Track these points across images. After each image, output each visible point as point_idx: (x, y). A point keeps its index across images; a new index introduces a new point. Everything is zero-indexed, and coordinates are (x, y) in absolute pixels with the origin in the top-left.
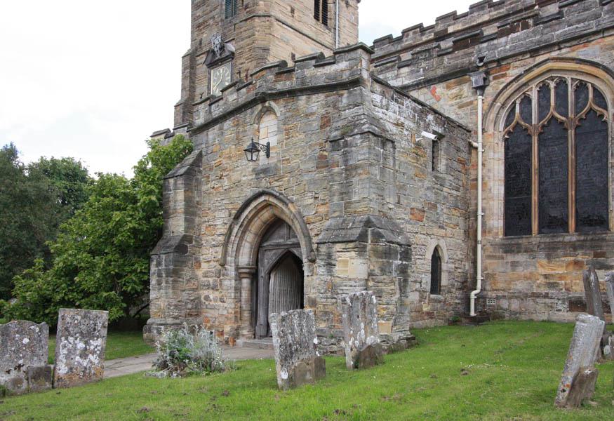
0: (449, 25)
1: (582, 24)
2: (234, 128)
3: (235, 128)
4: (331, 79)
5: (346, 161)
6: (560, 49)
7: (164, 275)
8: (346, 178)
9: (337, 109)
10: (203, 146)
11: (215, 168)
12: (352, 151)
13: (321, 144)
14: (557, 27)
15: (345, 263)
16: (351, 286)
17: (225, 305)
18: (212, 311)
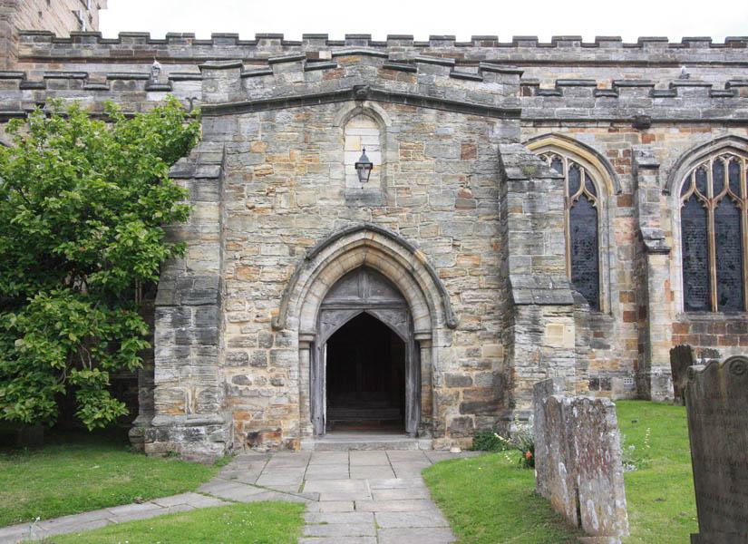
1: (579, 109)
3: (302, 125)
4: (476, 99)
5: (533, 208)
6: (561, 127)
7: (195, 341)
8: (534, 228)
9: (485, 138)
10: (229, 138)
11: (254, 177)
12: (540, 196)
13: (461, 179)
14: (557, 104)
15: (559, 329)
16: (568, 357)
17: (284, 389)
18: (255, 401)
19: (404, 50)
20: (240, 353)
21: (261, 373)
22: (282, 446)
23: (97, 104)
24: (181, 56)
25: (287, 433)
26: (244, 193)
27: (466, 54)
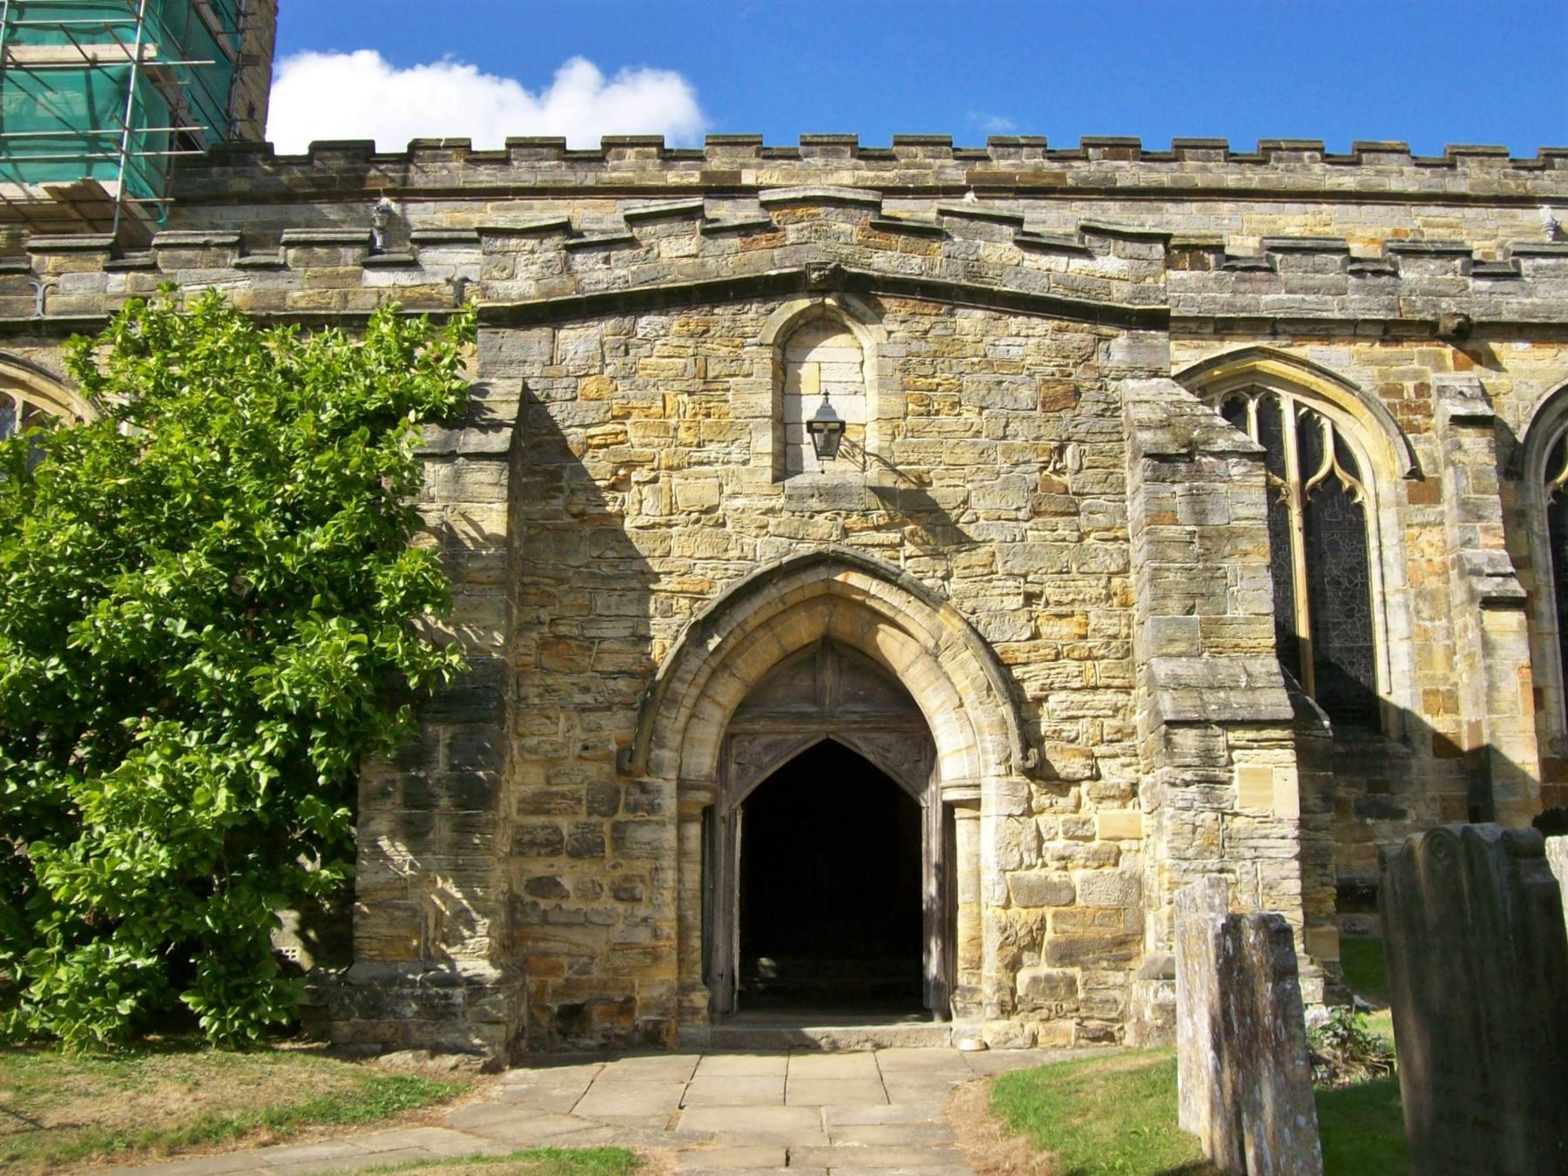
0: (745, 166)
1: (1311, 298)
2: (682, 342)
5: (1200, 515)
8: (1205, 556)
14: (1265, 287)
16: (1283, 838)
18: (576, 935)
19: (929, 167)
20: (544, 827)
21: (587, 868)
22: (637, 1037)
23: (256, 295)
24: (438, 186)
25: (647, 1007)
26: (563, 484)
27: (1069, 175)
